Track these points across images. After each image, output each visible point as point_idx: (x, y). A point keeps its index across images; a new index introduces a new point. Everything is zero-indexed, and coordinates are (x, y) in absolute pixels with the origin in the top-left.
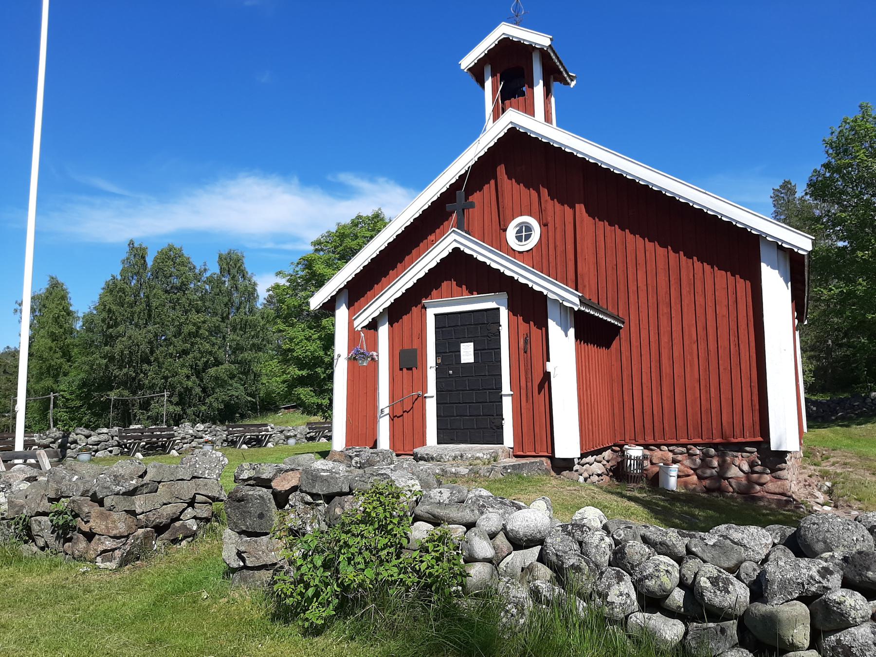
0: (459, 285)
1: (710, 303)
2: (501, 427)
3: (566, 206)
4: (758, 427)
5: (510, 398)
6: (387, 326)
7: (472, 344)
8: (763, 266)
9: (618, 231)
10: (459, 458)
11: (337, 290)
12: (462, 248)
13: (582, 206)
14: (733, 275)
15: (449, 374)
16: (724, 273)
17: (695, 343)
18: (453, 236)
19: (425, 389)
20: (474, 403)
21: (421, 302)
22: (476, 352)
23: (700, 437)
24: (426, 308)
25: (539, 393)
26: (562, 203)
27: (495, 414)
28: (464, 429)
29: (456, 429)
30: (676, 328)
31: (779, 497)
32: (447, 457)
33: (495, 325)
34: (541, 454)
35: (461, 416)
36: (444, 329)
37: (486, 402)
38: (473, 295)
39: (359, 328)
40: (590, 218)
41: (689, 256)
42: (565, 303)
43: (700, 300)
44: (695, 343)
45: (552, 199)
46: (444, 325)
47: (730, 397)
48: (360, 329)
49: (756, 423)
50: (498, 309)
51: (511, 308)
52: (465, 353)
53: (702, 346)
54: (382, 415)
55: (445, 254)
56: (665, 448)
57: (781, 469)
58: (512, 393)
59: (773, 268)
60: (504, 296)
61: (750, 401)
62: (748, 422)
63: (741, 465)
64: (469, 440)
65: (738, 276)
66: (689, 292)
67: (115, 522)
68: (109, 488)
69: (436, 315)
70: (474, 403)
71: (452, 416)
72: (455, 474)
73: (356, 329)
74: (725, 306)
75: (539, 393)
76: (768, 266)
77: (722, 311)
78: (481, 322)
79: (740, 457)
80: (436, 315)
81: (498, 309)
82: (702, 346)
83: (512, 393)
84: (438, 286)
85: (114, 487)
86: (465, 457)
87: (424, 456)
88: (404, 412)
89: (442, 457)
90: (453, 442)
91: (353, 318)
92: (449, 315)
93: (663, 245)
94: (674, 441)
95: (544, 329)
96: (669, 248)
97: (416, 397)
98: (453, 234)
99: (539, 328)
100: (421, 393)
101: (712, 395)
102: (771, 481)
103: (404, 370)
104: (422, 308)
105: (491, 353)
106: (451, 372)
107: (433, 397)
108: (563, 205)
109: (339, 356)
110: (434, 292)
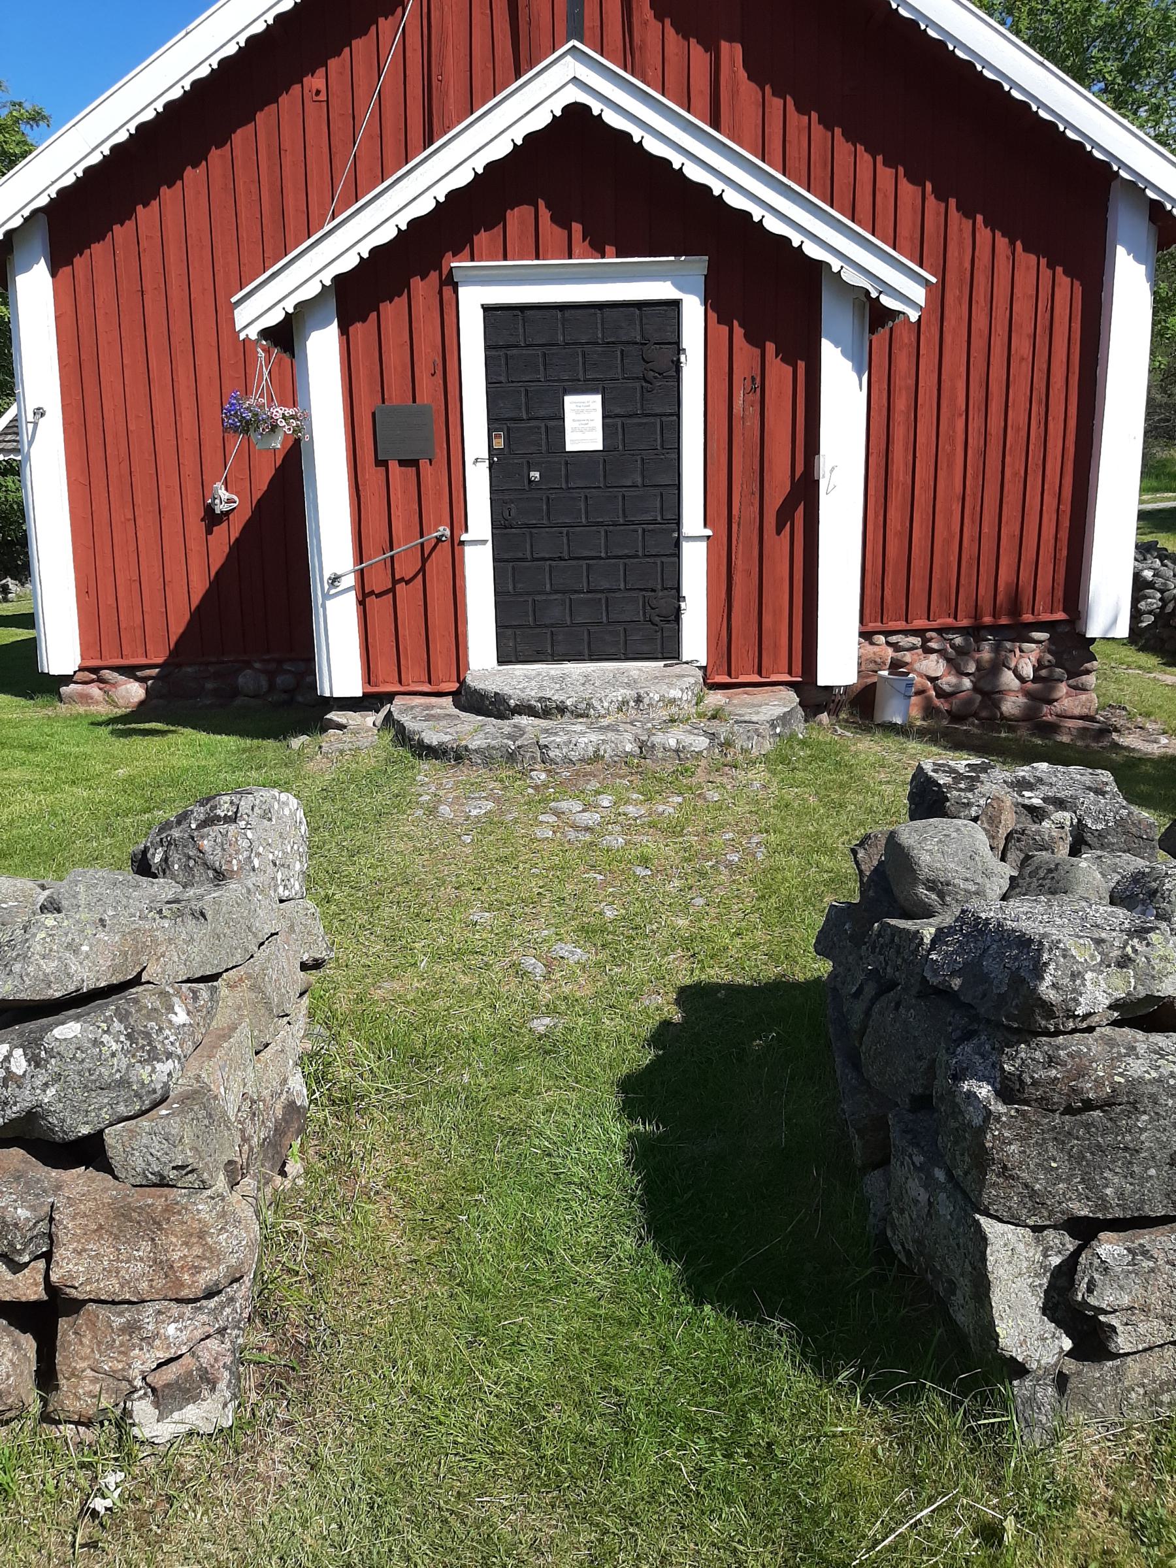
0: (562, 220)
1: (1000, 328)
2: (676, 616)
3: (693, 41)
4: (1060, 594)
5: (703, 545)
6: (333, 329)
7: (597, 399)
8: (1121, 251)
9: (818, 130)
10: (632, 704)
11: (26, 212)
12: (596, 108)
13: (738, 48)
14: (1051, 266)
15: (530, 481)
16: (1033, 257)
17: (961, 415)
18: (570, 67)
19: (458, 518)
20: (602, 559)
21: (439, 267)
22: (607, 421)
23: (952, 615)
24: (455, 287)
25: (779, 533)
26: (684, 31)
27: (659, 587)
28: (573, 625)
29: (552, 625)
30: (928, 380)
31: (1080, 723)
32: (606, 704)
33: (668, 350)
34: (774, 678)
35: (564, 592)
36: (515, 351)
37: (636, 556)
38: (603, 257)
39: (253, 333)
40: (753, 85)
41: (967, 212)
42: (886, 301)
43: (980, 321)
44: (961, 415)
45: (659, 17)
46: (512, 341)
47: (1017, 532)
48: (253, 336)
49: (1058, 584)
50: (676, 304)
51: (714, 300)
52: (576, 424)
53: (976, 424)
54: (332, 592)
55: (540, 121)
56: (881, 639)
57: (1088, 672)
58: (709, 532)
59: (1138, 259)
60: (698, 266)
61: (1053, 541)
62: (1044, 583)
63: (1020, 667)
64: (586, 651)
65: (1059, 270)
66: (960, 299)
67: (202, 1234)
68: (124, 1083)
69: (487, 309)
70: (602, 559)
71: (576, 592)
72: (677, 751)
73: (242, 336)
74: (1029, 336)
75: (779, 533)
76: (1129, 254)
77: (1022, 346)
78: (624, 339)
79: (1017, 651)
80: (487, 309)
81: (676, 304)
82: (976, 424)
83: (709, 532)
84: (495, 219)
85: (144, 1072)
86: (646, 701)
87: (533, 703)
88: (395, 582)
89: (590, 705)
90: (543, 658)
91: (233, 300)
92: (528, 313)
93: (915, 178)
94: (901, 625)
95: (801, 365)
96: (541, 203)
97: (433, 542)
98: (568, 58)
99: (789, 358)
100: (448, 532)
101: (985, 530)
102: (1068, 695)
103: (393, 466)
104: (442, 283)
105: (654, 424)
106: (535, 475)
107: (484, 542)
108: (686, 38)
109: (40, 412)
110: (482, 239)
